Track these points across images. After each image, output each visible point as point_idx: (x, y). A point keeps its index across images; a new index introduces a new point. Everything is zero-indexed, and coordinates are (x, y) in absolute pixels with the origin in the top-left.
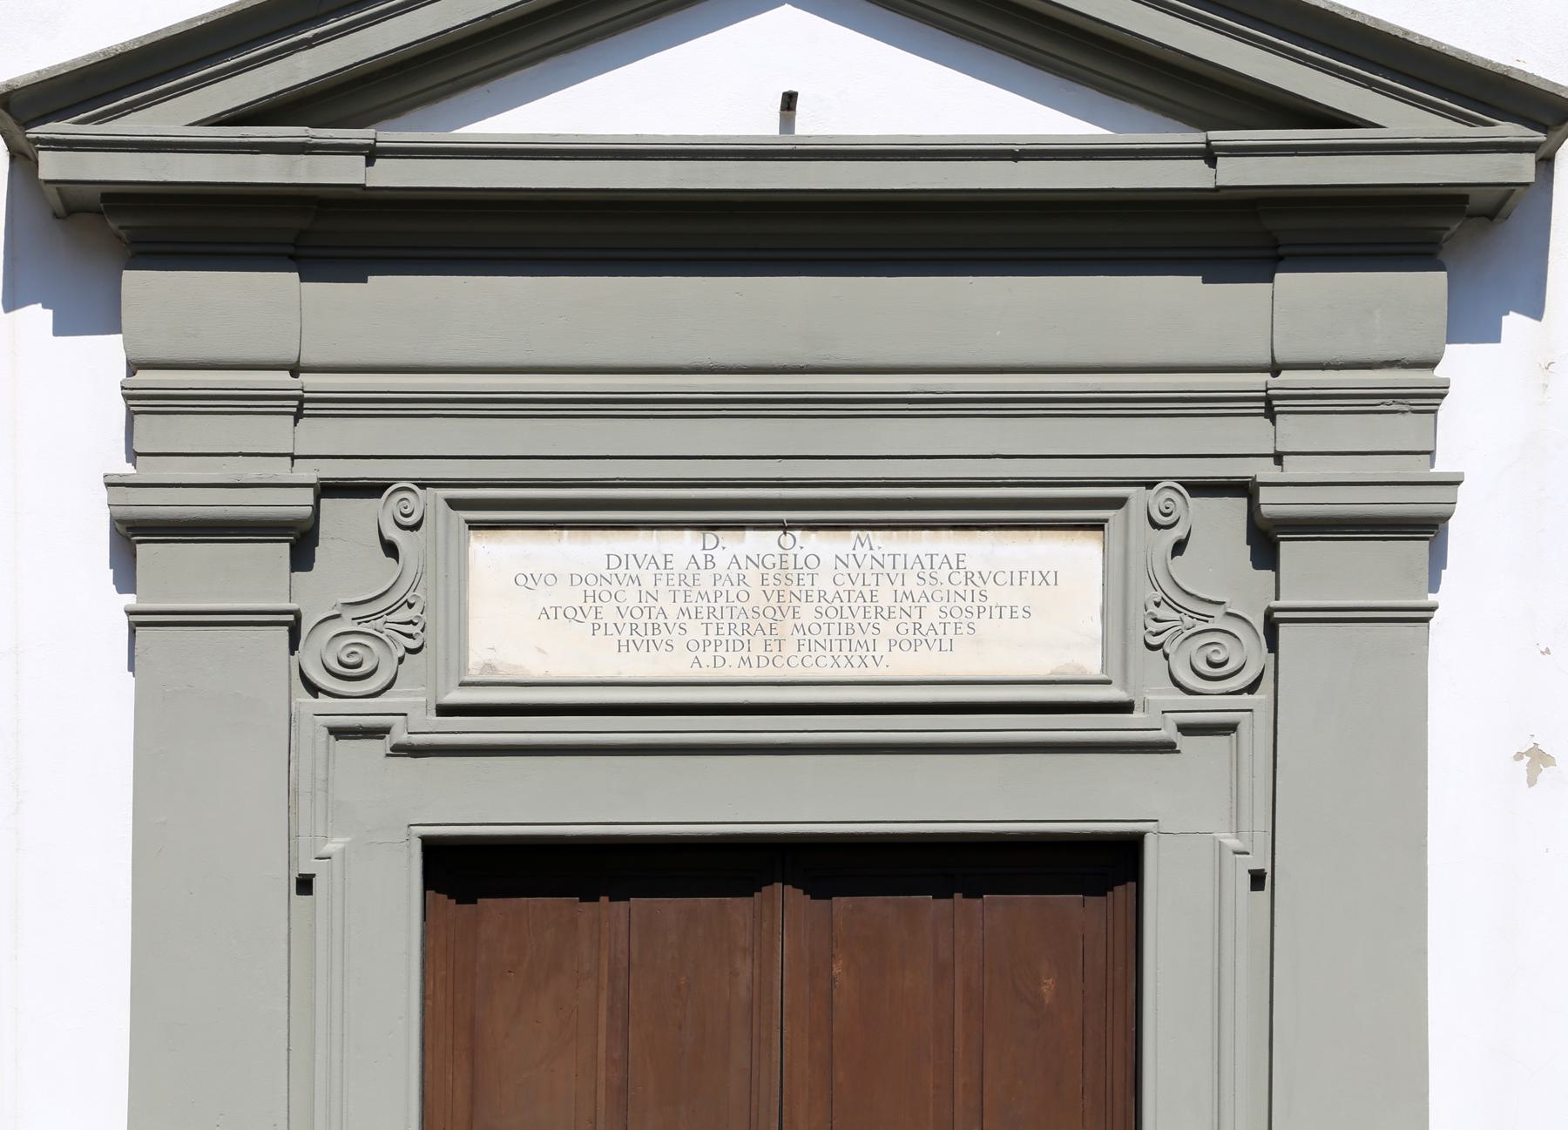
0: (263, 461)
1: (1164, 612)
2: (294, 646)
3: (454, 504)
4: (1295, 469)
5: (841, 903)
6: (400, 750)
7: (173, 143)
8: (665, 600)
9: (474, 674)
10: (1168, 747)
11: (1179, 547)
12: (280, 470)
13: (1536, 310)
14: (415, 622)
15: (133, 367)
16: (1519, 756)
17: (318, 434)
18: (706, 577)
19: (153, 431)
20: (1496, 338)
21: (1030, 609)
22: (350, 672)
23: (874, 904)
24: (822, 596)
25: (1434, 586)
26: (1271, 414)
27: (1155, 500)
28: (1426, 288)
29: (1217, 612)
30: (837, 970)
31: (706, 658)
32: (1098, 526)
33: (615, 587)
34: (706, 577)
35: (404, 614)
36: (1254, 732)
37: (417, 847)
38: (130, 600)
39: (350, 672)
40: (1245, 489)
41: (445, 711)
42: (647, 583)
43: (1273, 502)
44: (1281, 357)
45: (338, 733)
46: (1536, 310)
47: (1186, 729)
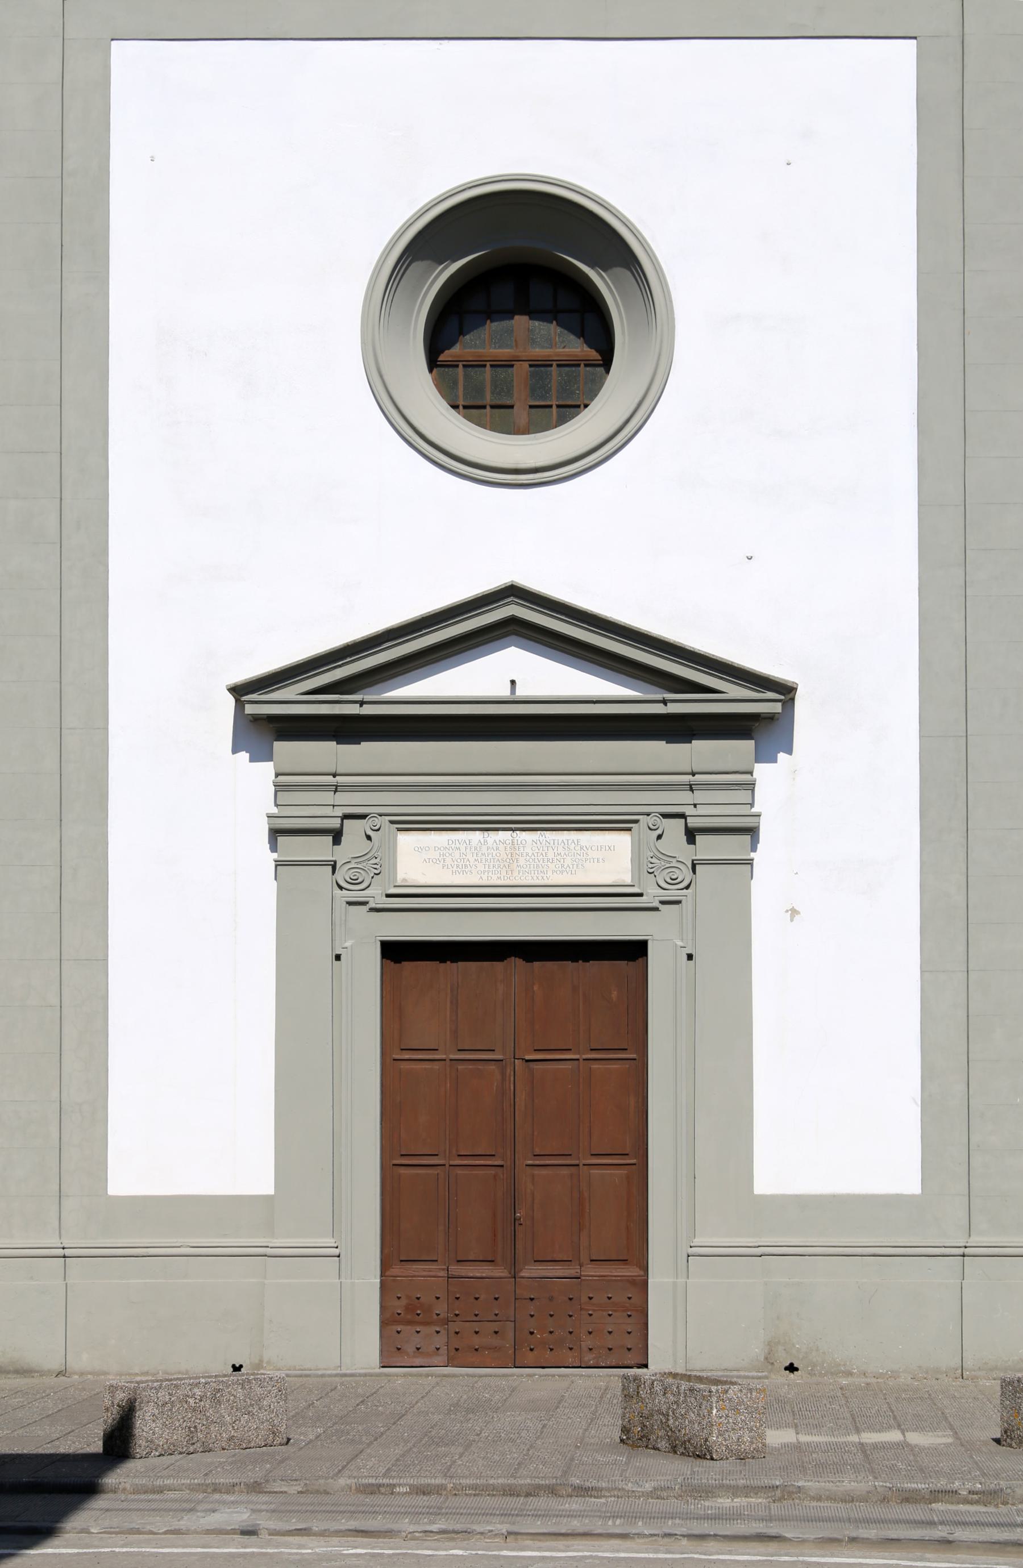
0: (325, 809)
1: (654, 860)
2: (334, 872)
3: (392, 822)
4: (701, 810)
5: (537, 964)
6: (372, 910)
7: (291, 701)
8: (470, 856)
9: (399, 883)
10: (656, 909)
11: (659, 837)
12: (328, 811)
13: (789, 751)
14: (381, 865)
15: (277, 775)
16: (787, 911)
17: (342, 798)
18: (484, 848)
19: (285, 797)
20: (776, 762)
21: (605, 859)
22: (354, 882)
23: (550, 964)
24: (527, 855)
25: (754, 849)
26: (692, 790)
27: (650, 820)
28: (747, 746)
29: (674, 860)
30: (536, 988)
31: (485, 877)
32: (629, 829)
33: (458, 845)
34: (484, 848)
35: (374, 861)
36: (687, 904)
37: (379, 944)
38: (275, 856)
39: (354, 882)
40: (682, 816)
41: (388, 896)
42: (463, 850)
43: (692, 822)
44: (695, 770)
45: (350, 903)
46: (789, 751)
47: (663, 903)
